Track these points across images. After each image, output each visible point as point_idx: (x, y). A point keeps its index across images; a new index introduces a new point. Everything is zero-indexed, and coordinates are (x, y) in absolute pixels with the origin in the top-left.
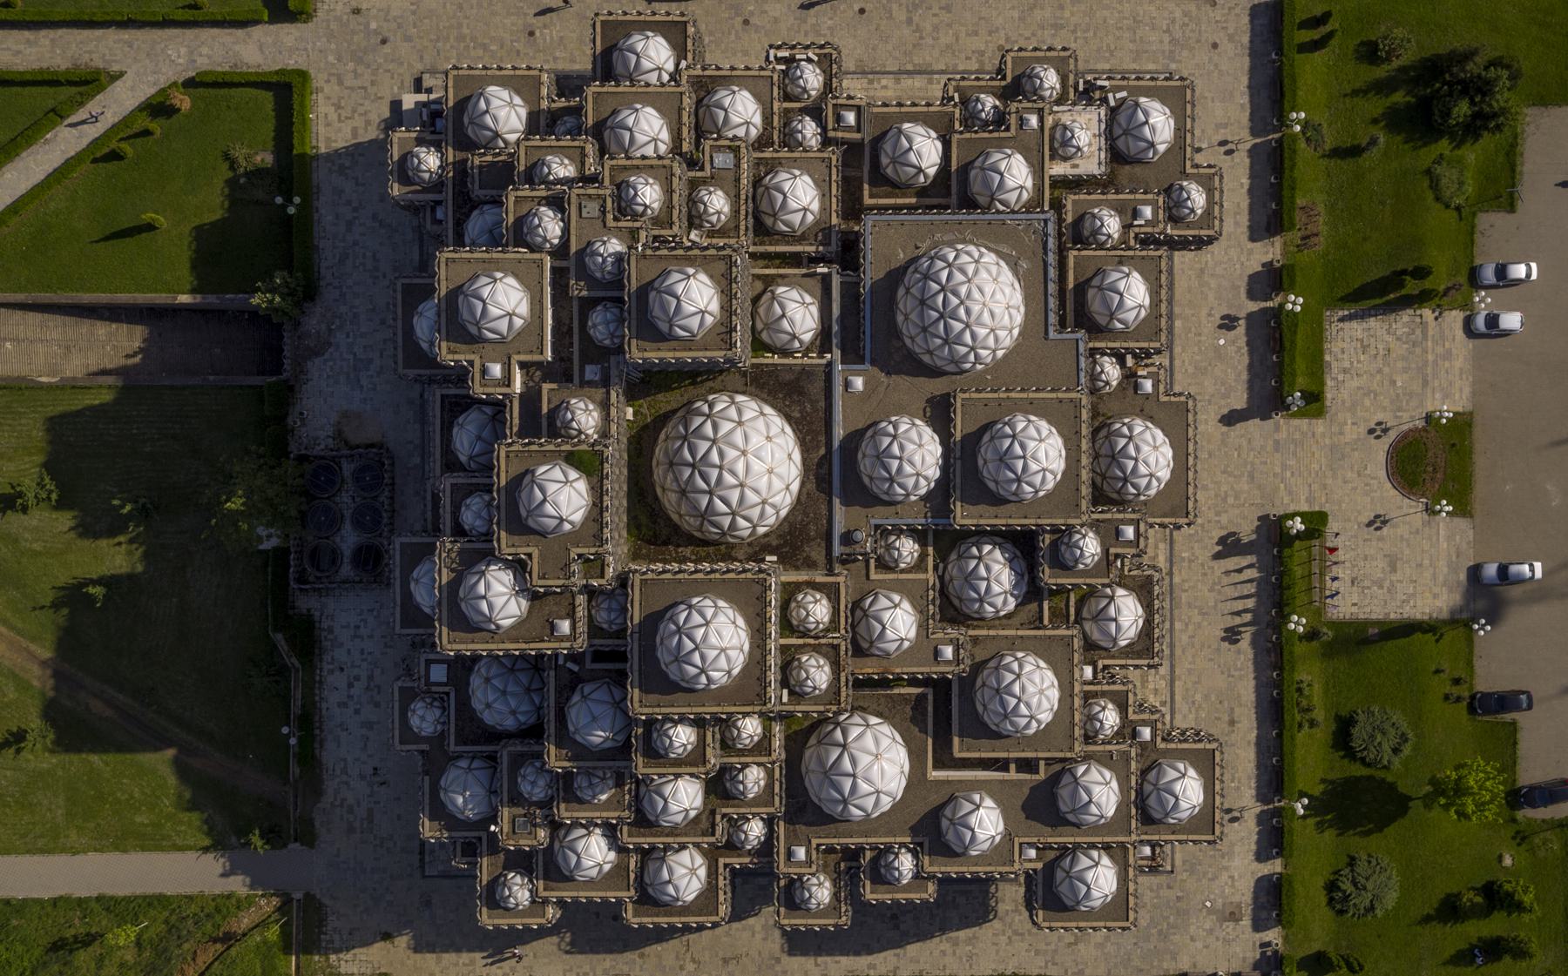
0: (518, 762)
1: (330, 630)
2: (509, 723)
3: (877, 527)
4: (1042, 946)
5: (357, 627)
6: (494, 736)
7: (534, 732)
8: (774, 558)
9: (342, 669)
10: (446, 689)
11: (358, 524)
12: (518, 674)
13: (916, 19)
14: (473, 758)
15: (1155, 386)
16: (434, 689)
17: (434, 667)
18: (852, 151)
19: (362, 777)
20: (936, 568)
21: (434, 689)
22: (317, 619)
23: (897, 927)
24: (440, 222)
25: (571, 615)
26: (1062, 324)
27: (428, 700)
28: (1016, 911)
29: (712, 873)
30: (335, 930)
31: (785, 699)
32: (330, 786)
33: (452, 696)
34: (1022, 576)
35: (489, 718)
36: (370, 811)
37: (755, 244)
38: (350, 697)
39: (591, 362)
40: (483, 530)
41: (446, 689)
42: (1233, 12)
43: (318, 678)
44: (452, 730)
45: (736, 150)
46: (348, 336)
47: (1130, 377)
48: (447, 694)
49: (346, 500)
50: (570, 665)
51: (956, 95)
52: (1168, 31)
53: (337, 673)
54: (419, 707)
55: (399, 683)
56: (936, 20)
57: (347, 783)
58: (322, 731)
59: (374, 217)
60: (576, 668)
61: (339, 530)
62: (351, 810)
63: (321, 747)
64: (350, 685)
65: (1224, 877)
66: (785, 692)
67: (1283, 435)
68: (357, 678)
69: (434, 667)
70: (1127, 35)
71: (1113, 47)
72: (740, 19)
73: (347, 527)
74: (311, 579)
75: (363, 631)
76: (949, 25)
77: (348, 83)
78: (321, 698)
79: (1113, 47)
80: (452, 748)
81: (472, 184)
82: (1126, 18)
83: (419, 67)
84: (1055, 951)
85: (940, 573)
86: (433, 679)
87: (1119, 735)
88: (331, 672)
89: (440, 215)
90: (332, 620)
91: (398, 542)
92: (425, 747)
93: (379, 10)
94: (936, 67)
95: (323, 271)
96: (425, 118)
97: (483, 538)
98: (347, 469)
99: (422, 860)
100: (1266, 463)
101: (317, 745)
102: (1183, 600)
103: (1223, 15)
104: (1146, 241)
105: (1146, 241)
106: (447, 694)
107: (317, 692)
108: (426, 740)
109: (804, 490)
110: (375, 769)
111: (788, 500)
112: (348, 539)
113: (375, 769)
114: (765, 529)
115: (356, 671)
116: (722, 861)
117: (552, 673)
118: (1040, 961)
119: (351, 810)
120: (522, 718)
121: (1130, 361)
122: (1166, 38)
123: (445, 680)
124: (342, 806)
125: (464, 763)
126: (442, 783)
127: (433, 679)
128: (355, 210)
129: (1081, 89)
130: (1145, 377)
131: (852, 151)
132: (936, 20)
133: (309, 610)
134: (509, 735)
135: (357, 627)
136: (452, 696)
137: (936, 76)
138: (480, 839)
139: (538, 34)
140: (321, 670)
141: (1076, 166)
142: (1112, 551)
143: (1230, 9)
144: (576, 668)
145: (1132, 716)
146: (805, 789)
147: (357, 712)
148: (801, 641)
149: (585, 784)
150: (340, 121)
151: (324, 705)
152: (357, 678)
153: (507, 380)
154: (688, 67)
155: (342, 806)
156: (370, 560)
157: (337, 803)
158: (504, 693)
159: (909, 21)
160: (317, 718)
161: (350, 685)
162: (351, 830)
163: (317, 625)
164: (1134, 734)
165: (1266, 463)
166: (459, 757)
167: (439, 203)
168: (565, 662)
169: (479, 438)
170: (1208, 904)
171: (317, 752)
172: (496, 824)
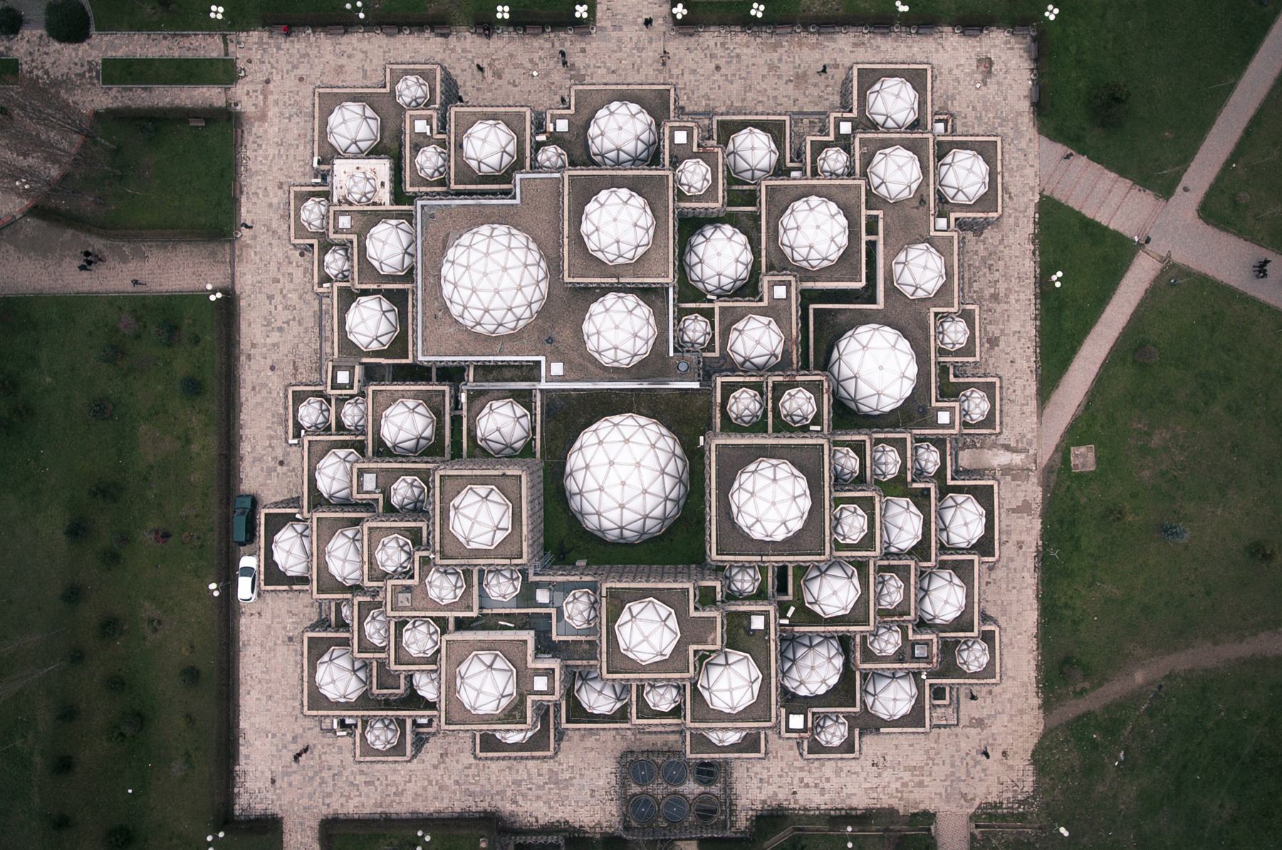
0: (868, 656)
1: (764, 802)
2: (839, 662)
3: (516, 86)
4: (1012, 220)
5: (761, 780)
6: (847, 674)
7: (845, 644)
8: (702, 438)
9: (795, 793)
10: (810, 715)
11: (680, 781)
12: (797, 657)
13: (279, 324)
14: (866, 692)
15: (562, 117)
16: (810, 725)
17: (792, 726)
18: (372, 374)
19: (880, 775)
20: (711, 301)
21: (810, 725)
22: (754, 813)
23: (997, 339)
24: (431, 721)
25: (748, 615)
26: (506, 193)
27: (819, 730)
28: (984, 242)
29: (960, 490)
30: (999, 797)
31: (818, 428)
32: (886, 802)
33: (815, 710)
34: (716, 227)
35: (834, 680)
36: (907, 769)
37: (443, 455)
38: (816, 786)
39: (534, 598)
40: (674, 692)
41: (810, 715)
42: (276, 65)
43: (801, 812)
44: (843, 709)
45: (361, 472)
46: (530, 789)
47: (555, 139)
48: (814, 714)
49: (659, 789)
50: (789, 614)
51: (325, 285)
52: (290, 118)
53: (798, 796)
54: (823, 738)
55: (805, 753)
56: (280, 308)
57: (884, 788)
58: (843, 809)
59: (435, 767)
60: (792, 609)
61: (683, 796)
62: (905, 785)
63: (856, 809)
64: (807, 786)
65: (955, 72)
66: (812, 428)
67: (608, 24)
68: (801, 780)
69: (792, 726)
70: (292, 152)
71: (302, 163)
72: (279, 468)
73: (680, 789)
74: (722, 818)
75: (765, 776)
76: (284, 296)
77: (329, 790)
78: (818, 809)
79: (302, 163)
80: (857, 709)
81: (396, 695)
82: (279, 151)
83: (318, 729)
84: (1016, 210)
85: (715, 298)
86: (801, 726)
87: (847, 149)
88: (796, 802)
89: (425, 721)
90: (755, 800)
91: (689, 755)
92: (857, 732)
93: (272, 764)
94: (317, 308)
95: (479, 809)
96: (345, 733)
97: (682, 691)
98: (635, 789)
99: (945, 726)
100: (631, 38)
101: (854, 813)
102: (740, 105)
103: (277, 73)
104: (443, 126)
105: (443, 126)
106: (814, 714)
107: (812, 813)
108: (851, 730)
109: (646, 412)
110: (873, 765)
111: (653, 427)
112: (691, 788)
113: (873, 765)
114: (677, 447)
115: (796, 781)
116: (950, 482)
117: (796, 629)
118: (1023, 221)
119: (905, 785)
120: (833, 652)
121: (542, 138)
122: (295, 119)
123: (802, 717)
124: (902, 792)
125: (870, 700)
126: (886, 717)
127: (801, 726)
128: (430, 783)
129: (319, 180)
130: (555, 125)
131: (372, 374)
132: (280, 308)
133: (747, 820)
134: (847, 664)
135: (761, 780)
136: (815, 710)
137: (324, 307)
138: (931, 685)
139: (291, 634)
140: (794, 809)
141: (383, 184)
142: (695, 149)
143: (273, 68)
144: (792, 609)
145: (831, 138)
146: (892, 411)
147: (828, 780)
148: (770, 415)
149: (888, 599)
150: (360, 795)
151: (823, 807)
152: (801, 780)
153: (549, 673)
154: (302, 513)
155: (902, 792)
156: (707, 772)
157: (900, 795)
158: (813, 668)
159: (280, 329)
160: (832, 813)
161: (807, 786)
162: (920, 784)
163: (759, 813)
164: (847, 136)
165: (631, 38)
166: (864, 703)
167: (414, 722)
168: (787, 618)
169: (600, 692)
170: (978, 86)
171: (859, 812)
172: (920, 673)
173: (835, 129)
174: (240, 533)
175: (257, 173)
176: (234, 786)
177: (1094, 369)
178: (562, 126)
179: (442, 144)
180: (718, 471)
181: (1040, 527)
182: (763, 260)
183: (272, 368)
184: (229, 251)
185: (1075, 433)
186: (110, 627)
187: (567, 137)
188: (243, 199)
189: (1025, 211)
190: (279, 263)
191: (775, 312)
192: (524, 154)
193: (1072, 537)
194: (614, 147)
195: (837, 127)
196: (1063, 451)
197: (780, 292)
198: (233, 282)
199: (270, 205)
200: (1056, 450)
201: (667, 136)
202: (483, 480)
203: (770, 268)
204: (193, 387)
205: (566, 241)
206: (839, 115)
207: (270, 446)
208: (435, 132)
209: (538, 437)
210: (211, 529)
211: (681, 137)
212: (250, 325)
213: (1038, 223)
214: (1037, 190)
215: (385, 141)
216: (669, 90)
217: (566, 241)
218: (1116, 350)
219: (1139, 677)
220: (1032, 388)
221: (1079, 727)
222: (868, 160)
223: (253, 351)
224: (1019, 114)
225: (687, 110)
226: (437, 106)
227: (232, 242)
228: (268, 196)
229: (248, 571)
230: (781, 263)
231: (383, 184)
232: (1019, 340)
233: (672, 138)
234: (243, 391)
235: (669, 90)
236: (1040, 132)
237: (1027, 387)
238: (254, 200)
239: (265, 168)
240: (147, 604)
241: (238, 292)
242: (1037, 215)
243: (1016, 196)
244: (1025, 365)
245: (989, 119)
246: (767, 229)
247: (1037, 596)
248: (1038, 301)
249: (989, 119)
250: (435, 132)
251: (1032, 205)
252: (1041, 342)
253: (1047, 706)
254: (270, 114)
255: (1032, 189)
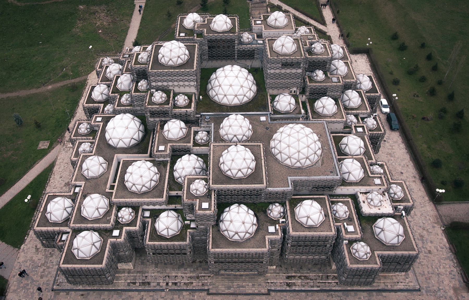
15: (272, 234)
173: (122, 233)
174: (393, 116)
175: (446, 259)
176: (369, 60)
177: (25, 177)
178: (271, 229)
179: (337, 220)
180: (193, 63)
181: (70, 125)
182: (168, 168)
183: (402, 173)
184: (444, 221)
185: (45, 153)
186: (432, 92)
187: (269, 224)
188: (447, 245)
189: (31, 240)
190: (416, 215)
191: (165, 141)
192: (291, 212)
193: (58, 122)
194: (237, 171)
195: (120, 234)
196: (51, 147)
197: (162, 148)
198: (436, 208)
199: (431, 242)
200: (54, 148)
201: (213, 206)
202: (311, 228)
203: (165, 166)
204: (436, 164)
205: (263, 158)
206: (119, 240)
207: (392, 146)
208: (342, 226)
209: (269, 101)
210: (406, 121)
211: (205, 205)
212: (420, 189)
213: (27, 234)
214: (21, 250)
215: (369, 227)
216: (212, 248)
217: (263, 158)
218: (12, 184)
219: (50, 87)
220: (55, 169)
221: (77, 75)
222: (108, 213)
223: (414, 179)
224: (15, 291)
225: (206, 293)
226: (345, 242)
227: (444, 225)
228: (435, 247)
229: (385, 106)
230: (159, 165)
231: (364, 202)
232: (55, 185)
233: (210, 205)
234: (412, 164)
235: (212, 248)
236: (7, 281)
237: (58, 168)
238: (441, 245)
239: (442, 261)
240: (422, 101)
241: (431, 203)
242: (26, 238)
243: (32, 248)
244: (56, 176)
245: (33, 289)
246: (165, 180)
247: (78, 106)
248: (40, 201)
249: (33, 289)
250: (342, 226)
251: (26, 243)
252: (45, 185)
253: (86, 80)
254: (452, 292)
255: (23, 250)
